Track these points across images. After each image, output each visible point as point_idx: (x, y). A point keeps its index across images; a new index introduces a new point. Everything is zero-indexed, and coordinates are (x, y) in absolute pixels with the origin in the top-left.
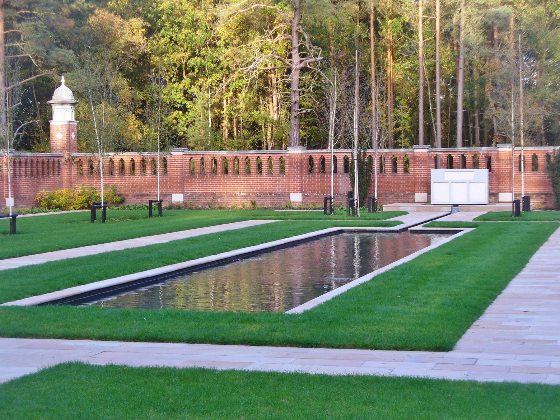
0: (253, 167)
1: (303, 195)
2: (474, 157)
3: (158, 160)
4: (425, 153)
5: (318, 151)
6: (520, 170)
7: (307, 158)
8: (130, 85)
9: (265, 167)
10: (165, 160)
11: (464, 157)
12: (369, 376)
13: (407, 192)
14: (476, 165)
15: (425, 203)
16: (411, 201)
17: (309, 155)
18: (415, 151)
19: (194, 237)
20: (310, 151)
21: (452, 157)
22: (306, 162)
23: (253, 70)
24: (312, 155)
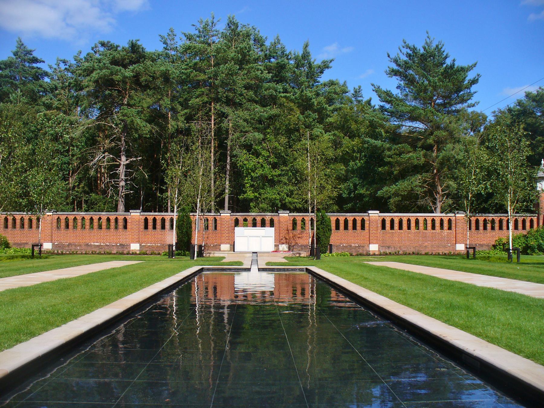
0: (350, 224)
1: (140, 245)
2: (66, 219)
3: (10, 218)
4: (228, 216)
5: (152, 214)
6: (173, 229)
7: (292, 219)
8: (377, 146)
9: (71, 223)
10: (216, 220)
11: (254, 219)
12: (39, 356)
13: (215, 244)
14: (263, 224)
15: (276, 252)
16: (218, 250)
17: (145, 216)
18: (280, 215)
19: (156, 282)
20: (146, 214)
21: (127, 219)
22: (143, 221)
23: (311, 146)
24: (442, 217)
